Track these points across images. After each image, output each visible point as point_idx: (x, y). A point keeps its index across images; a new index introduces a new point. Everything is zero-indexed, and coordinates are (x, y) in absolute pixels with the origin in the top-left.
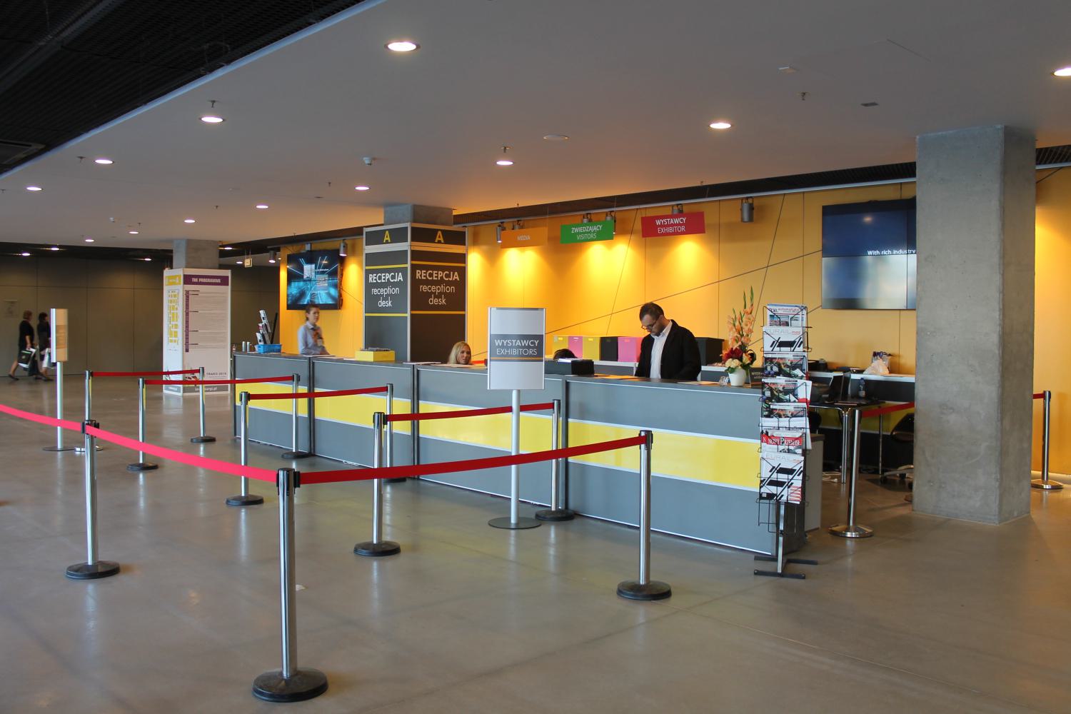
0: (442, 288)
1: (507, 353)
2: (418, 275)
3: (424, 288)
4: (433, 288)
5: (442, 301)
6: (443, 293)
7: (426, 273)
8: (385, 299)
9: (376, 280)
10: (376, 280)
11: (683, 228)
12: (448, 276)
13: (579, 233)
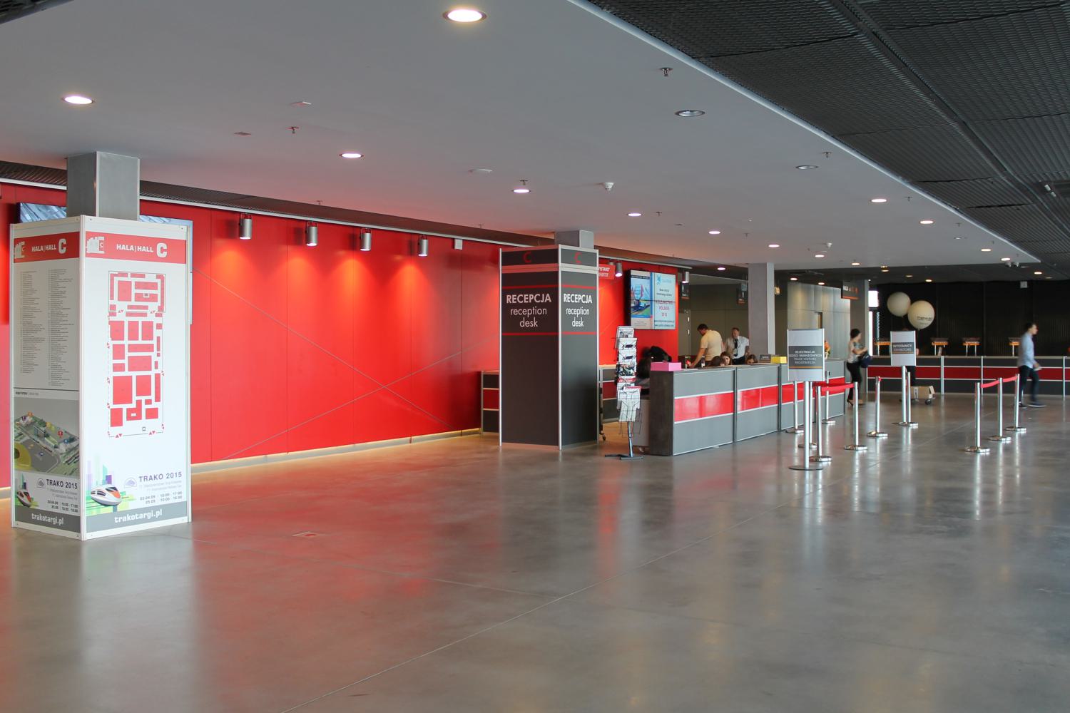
0: (534, 310)
2: (508, 300)
3: (515, 312)
4: (524, 311)
6: (535, 315)
8: (578, 319)
9: (570, 300)
10: (570, 300)
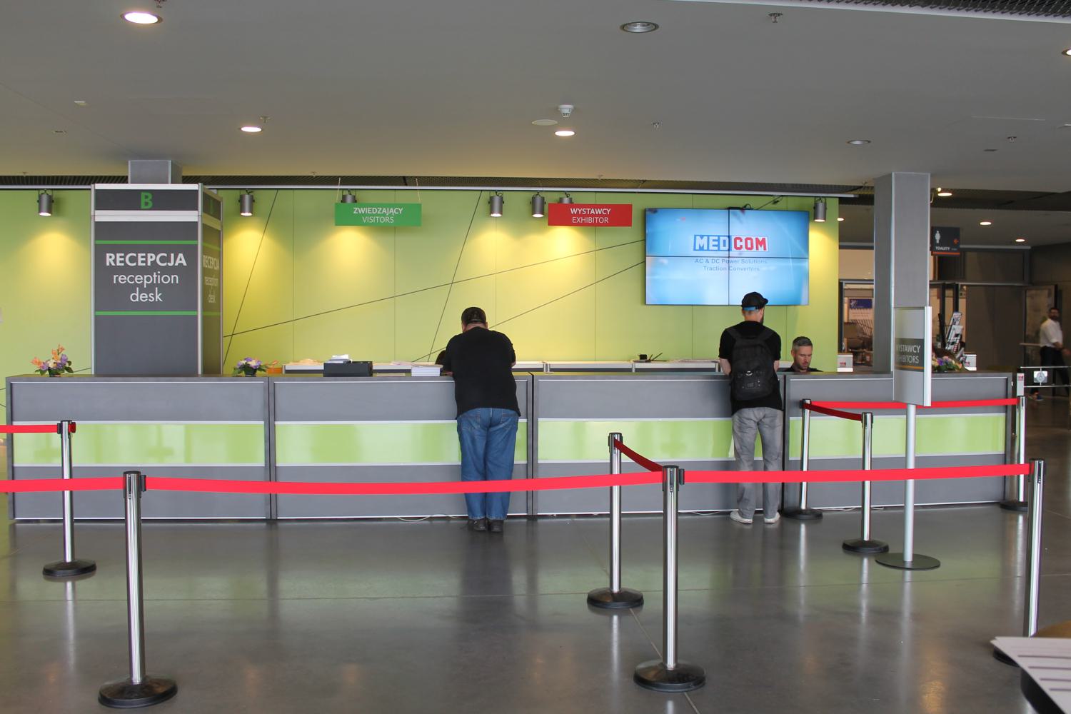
1: (583, 221)
3: (122, 279)
5: (154, 296)
6: (157, 285)
7: (124, 257)
11: (606, 220)
12: (166, 259)
13: (365, 215)
